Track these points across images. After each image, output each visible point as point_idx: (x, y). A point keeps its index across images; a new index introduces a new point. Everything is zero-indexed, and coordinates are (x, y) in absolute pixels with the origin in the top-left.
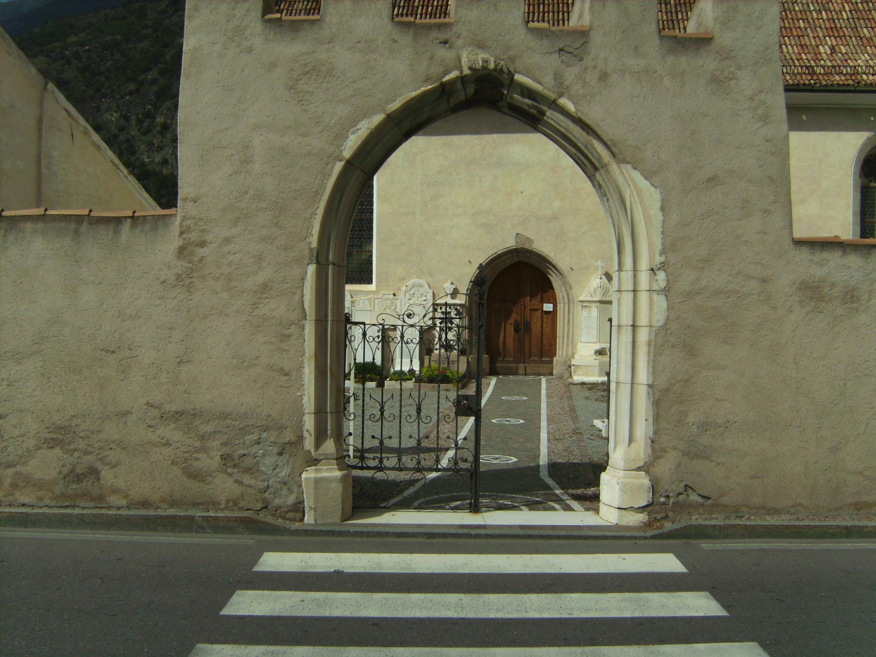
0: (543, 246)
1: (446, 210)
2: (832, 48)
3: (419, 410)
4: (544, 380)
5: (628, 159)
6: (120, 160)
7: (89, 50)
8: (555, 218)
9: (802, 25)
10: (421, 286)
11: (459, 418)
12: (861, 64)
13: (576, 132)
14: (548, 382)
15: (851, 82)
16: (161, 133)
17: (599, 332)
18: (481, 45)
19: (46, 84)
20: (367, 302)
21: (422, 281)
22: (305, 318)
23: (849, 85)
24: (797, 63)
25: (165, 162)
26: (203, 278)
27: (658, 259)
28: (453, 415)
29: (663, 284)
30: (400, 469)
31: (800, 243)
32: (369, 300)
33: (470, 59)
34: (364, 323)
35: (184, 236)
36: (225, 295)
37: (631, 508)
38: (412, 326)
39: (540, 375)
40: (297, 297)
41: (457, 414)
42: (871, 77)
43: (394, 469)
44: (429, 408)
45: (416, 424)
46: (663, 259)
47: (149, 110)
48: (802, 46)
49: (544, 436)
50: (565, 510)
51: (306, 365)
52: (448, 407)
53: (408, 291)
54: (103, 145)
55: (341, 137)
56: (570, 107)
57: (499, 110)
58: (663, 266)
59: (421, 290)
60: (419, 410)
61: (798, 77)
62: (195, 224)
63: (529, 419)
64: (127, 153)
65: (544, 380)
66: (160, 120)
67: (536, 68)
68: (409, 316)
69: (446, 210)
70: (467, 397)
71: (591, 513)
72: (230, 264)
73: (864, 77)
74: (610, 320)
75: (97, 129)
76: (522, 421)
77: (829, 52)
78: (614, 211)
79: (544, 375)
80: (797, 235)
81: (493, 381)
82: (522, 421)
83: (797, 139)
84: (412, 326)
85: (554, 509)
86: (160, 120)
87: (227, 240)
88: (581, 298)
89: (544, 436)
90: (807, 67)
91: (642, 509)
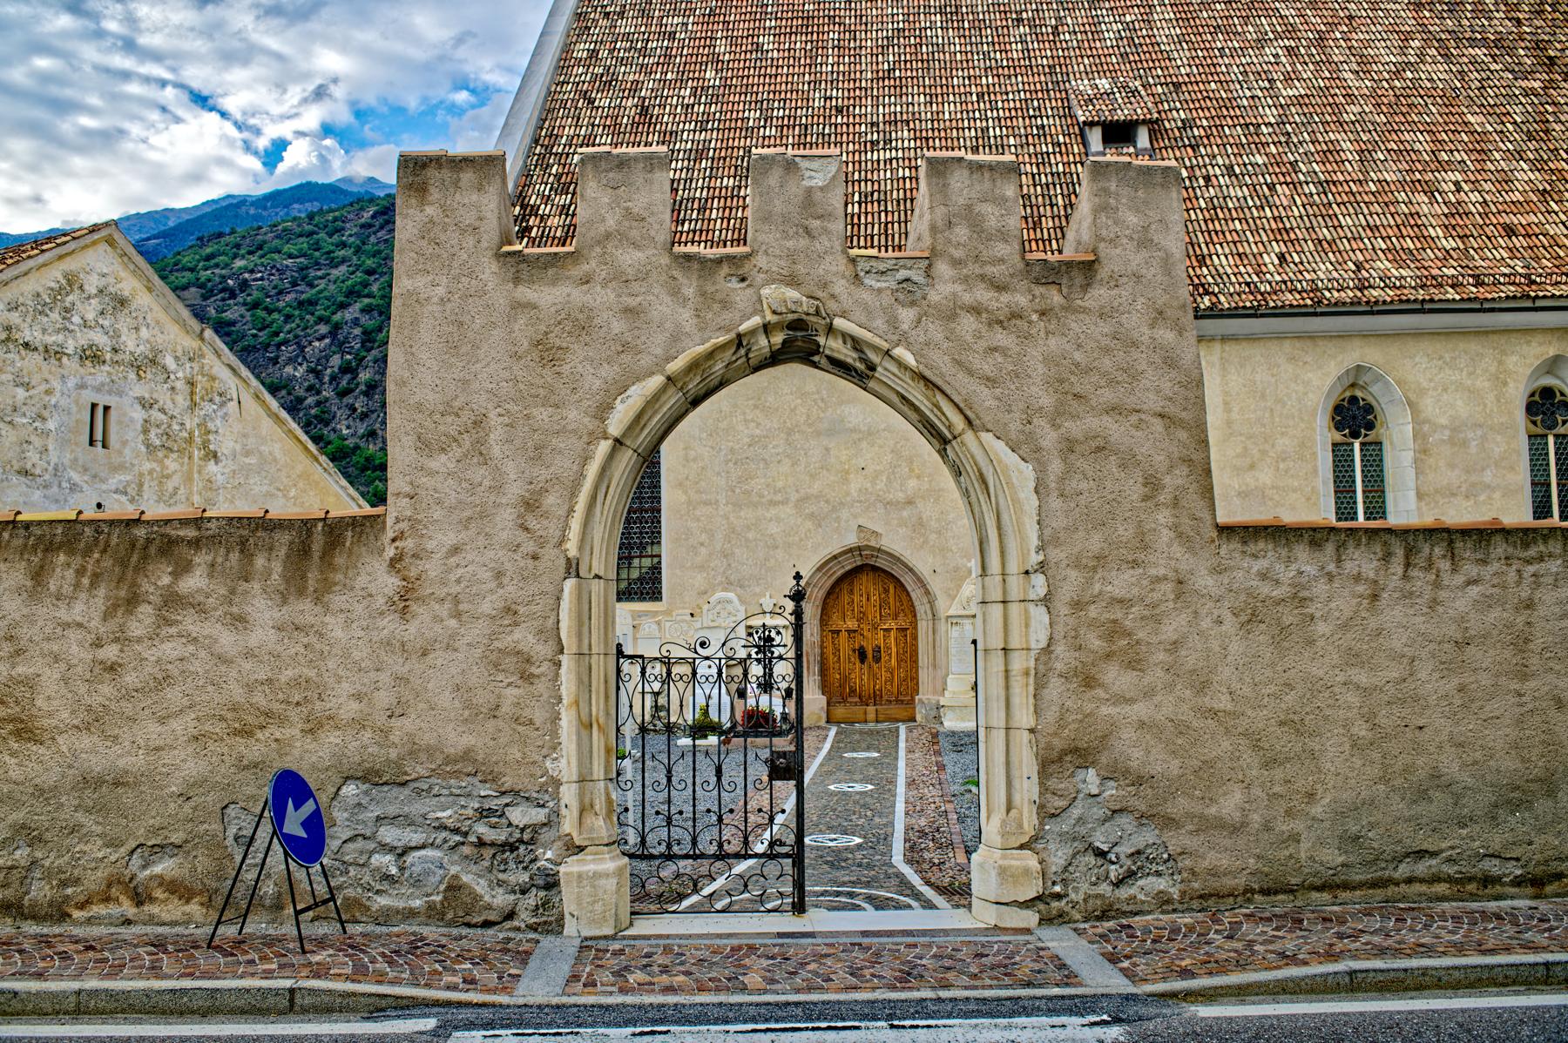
0: (894, 541)
1: (780, 486)
2: (1281, 257)
3: (719, 772)
4: (902, 728)
5: (989, 426)
6: (307, 433)
7: (262, 279)
8: (910, 502)
9: (1238, 227)
10: (729, 602)
11: (777, 783)
12: (1322, 276)
13: (917, 394)
14: (910, 730)
15: (1309, 302)
16: (366, 394)
17: (977, 664)
18: (792, 281)
19: (202, 331)
20: (655, 627)
21: (731, 595)
22: (561, 651)
23: (1306, 306)
24: (1233, 279)
25: (372, 434)
26: (421, 600)
27: (1035, 558)
28: (765, 778)
29: (1042, 592)
30: (695, 857)
31: (1226, 531)
32: (659, 623)
33: (780, 296)
34: (641, 657)
35: (397, 543)
36: (453, 623)
37: (1016, 903)
38: (707, 658)
39: (898, 721)
40: (551, 621)
41: (771, 779)
42: (1336, 294)
43: (687, 856)
44: (732, 772)
45: (715, 792)
46: (1041, 558)
47: (350, 362)
48: (1239, 255)
49: (900, 807)
50: (924, 907)
51: (563, 715)
52: (760, 771)
53: (720, 605)
54: (284, 414)
55: (603, 410)
56: (910, 359)
57: (815, 365)
58: (1042, 567)
59: (729, 607)
60: (719, 772)
61: (1236, 298)
62: (412, 527)
63: (863, 783)
64: (316, 426)
65: (902, 728)
66: (364, 376)
67: (859, 314)
68: (703, 645)
69: (780, 486)
70: (784, 754)
71: (962, 910)
72: (458, 581)
73: (1327, 294)
74: (974, 642)
75: (273, 390)
76: (870, 787)
77: (1276, 262)
78: (973, 499)
79: (903, 721)
80: (1222, 519)
81: (833, 731)
82: (870, 787)
83: (618, 605)
84: (707, 658)
85: (909, 907)
86: (364, 376)
87: (455, 550)
88: (951, 612)
89: (900, 807)
90: (1248, 284)
91: (1027, 904)
